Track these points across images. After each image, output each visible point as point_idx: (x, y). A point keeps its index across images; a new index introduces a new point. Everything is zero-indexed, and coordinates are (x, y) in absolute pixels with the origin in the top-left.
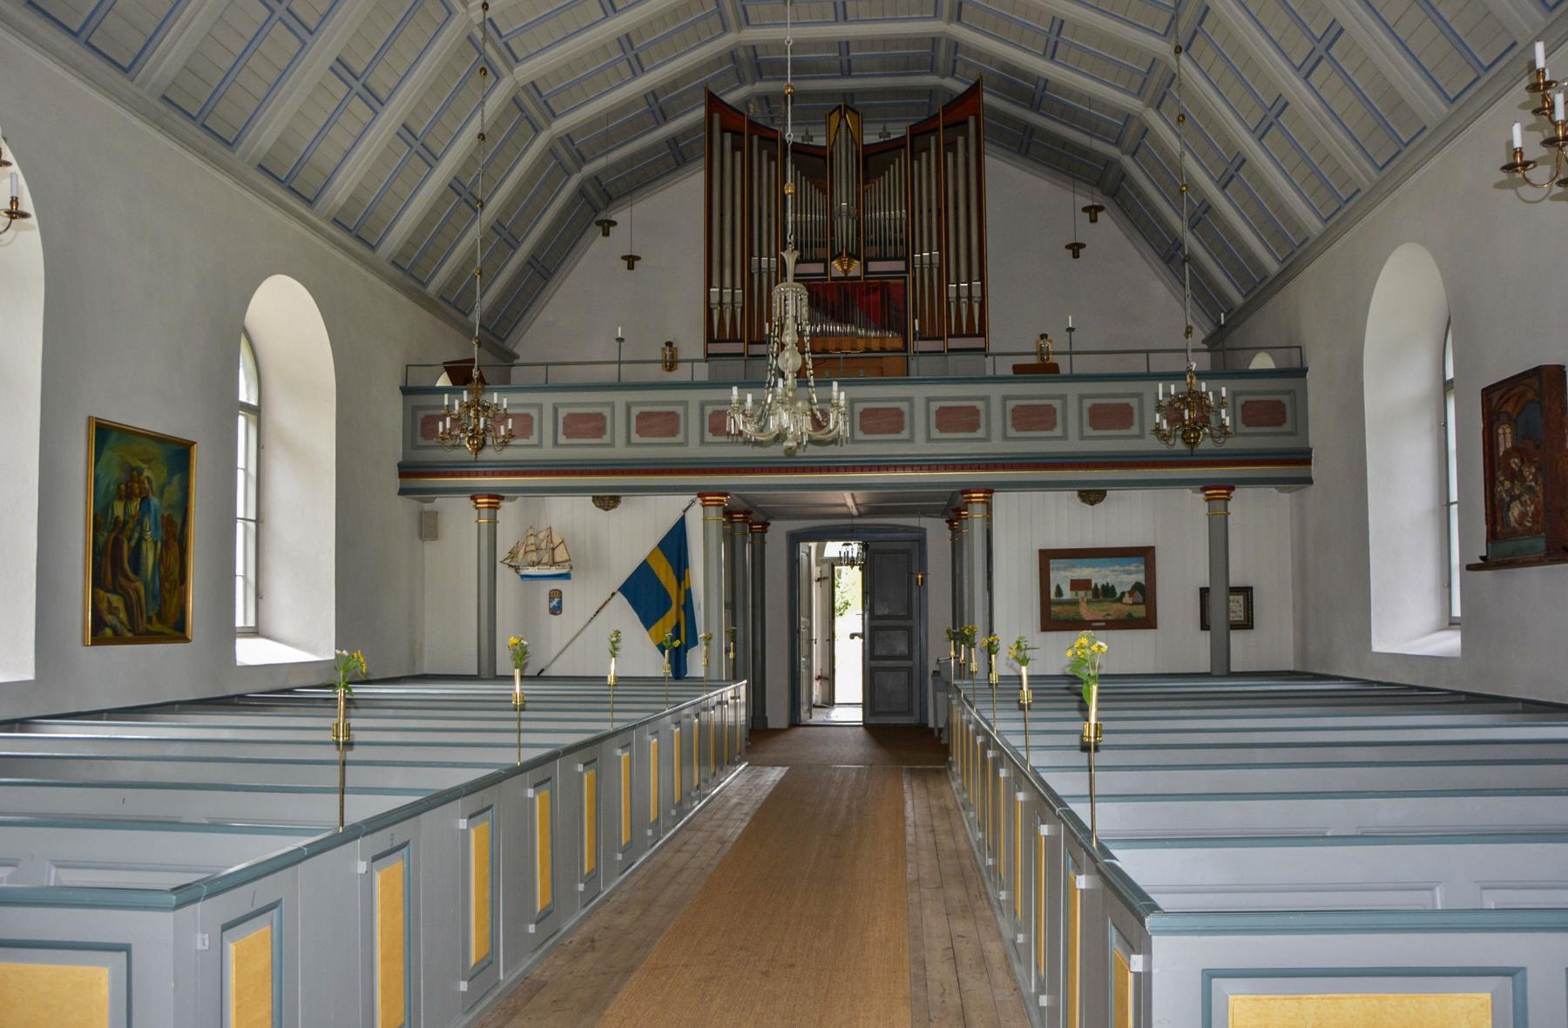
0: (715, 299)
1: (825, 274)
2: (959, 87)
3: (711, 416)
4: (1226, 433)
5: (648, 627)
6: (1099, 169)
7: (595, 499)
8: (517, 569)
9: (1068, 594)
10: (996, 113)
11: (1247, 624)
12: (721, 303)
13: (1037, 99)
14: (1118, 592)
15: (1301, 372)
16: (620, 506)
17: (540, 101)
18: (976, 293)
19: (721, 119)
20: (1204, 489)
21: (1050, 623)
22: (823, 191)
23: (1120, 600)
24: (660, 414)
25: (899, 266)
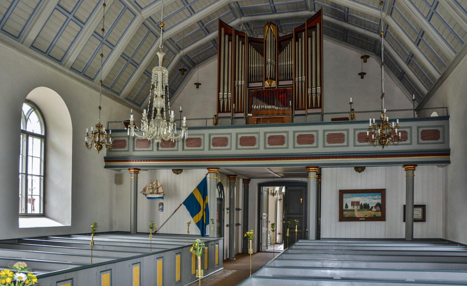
0: (221, 97)
1: (263, 86)
2: (313, 13)
3: (213, 139)
4: (399, 139)
5: (193, 217)
6: (366, 43)
7: (173, 170)
8: (146, 195)
9: (350, 207)
10: (328, 23)
11: (423, 219)
12: (223, 98)
13: (346, 16)
14: (370, 207)
15: (446, 118)
16: (182, 173)
17: (156, 25)
18: (319, 91)
19: (225, 30)
20: (404, 166)
21: (342, 218)
22: (262, 55)
23: (371, 210)
24: (194, 139)
25: (290, 82)
